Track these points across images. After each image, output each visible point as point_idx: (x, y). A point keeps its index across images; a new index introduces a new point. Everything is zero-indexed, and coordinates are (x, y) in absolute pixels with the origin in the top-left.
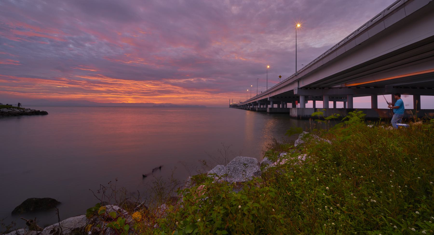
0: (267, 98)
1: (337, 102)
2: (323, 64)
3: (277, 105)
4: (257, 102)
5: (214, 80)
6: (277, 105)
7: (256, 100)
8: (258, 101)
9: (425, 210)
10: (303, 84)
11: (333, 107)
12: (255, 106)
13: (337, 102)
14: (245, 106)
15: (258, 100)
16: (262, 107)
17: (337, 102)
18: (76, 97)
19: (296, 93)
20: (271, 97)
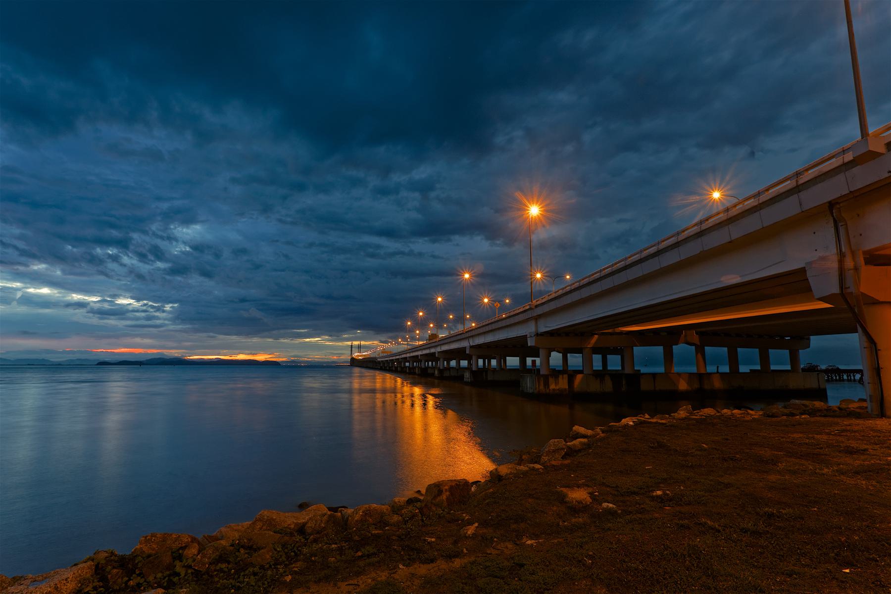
0: (465, 348)
1: (527, 358)
2: (542, 313)
3: (466, 362)
4: (437, 356)
5: (624, 383)
6: (466, 362)
7: (433, 350)
8: (439, 352)
9: (21, 268)
10: (546, 326)
11: (492, 360)
12: (415, 363)
13: (527, 358)
14: (389, 363)
15: (439, 349)
16: (479, 360)
17: (609, 357)
18: (300, 357)
19: (533, 344)
20: (473, 346)
